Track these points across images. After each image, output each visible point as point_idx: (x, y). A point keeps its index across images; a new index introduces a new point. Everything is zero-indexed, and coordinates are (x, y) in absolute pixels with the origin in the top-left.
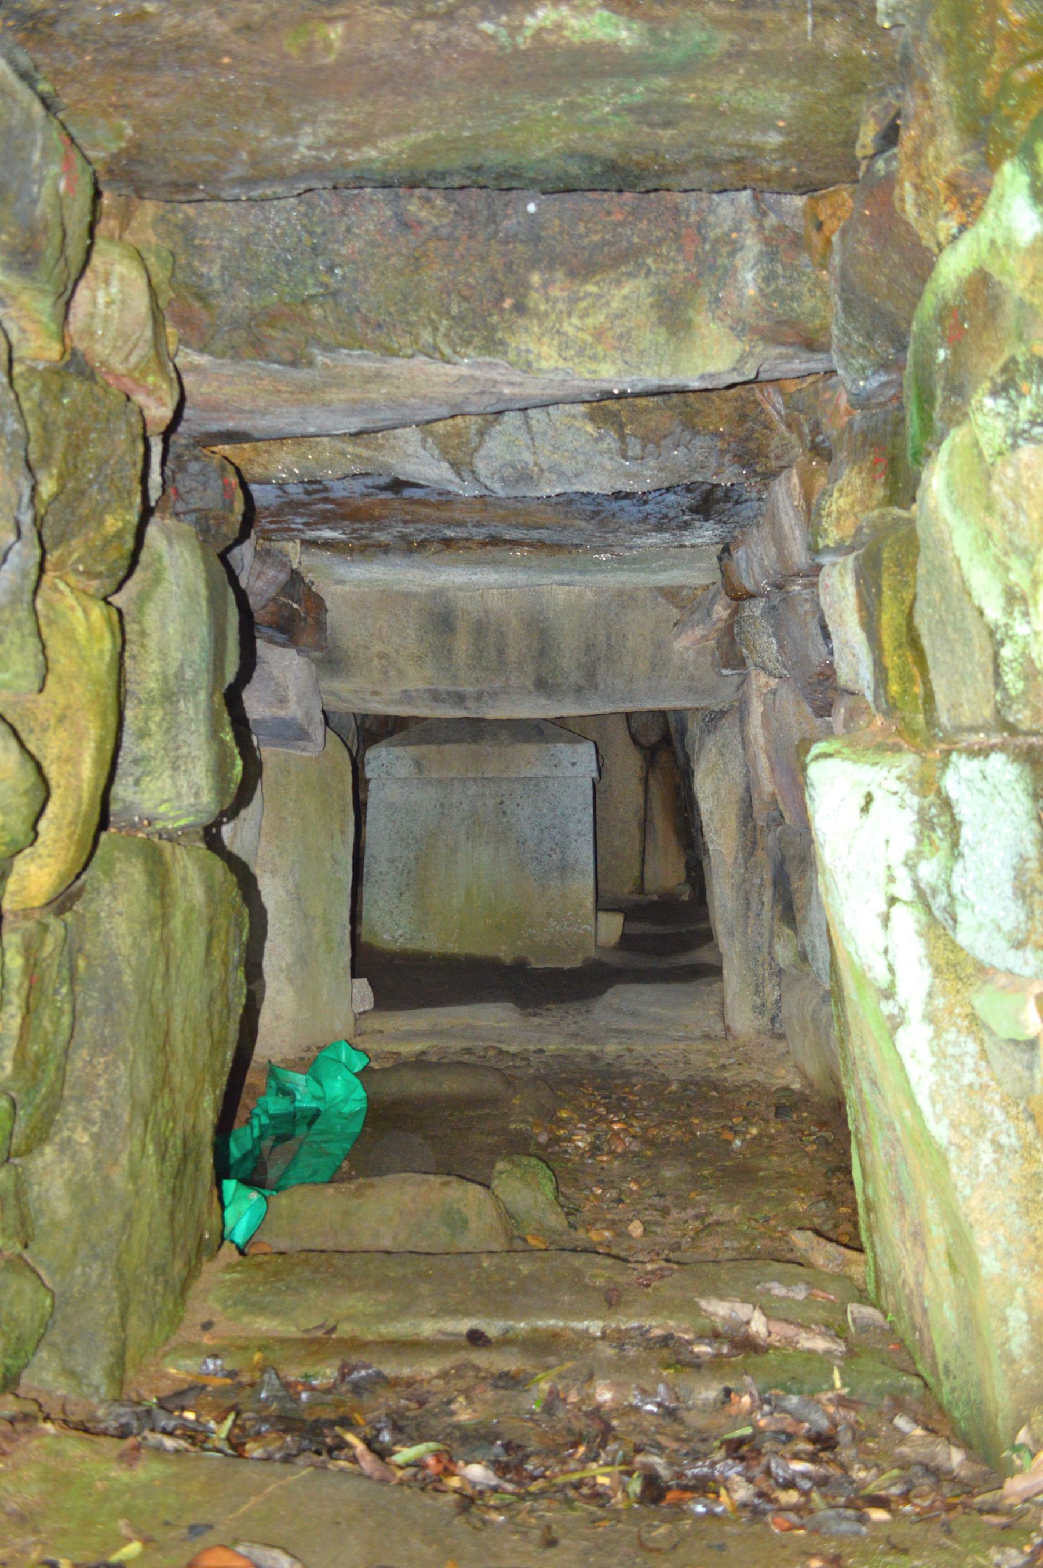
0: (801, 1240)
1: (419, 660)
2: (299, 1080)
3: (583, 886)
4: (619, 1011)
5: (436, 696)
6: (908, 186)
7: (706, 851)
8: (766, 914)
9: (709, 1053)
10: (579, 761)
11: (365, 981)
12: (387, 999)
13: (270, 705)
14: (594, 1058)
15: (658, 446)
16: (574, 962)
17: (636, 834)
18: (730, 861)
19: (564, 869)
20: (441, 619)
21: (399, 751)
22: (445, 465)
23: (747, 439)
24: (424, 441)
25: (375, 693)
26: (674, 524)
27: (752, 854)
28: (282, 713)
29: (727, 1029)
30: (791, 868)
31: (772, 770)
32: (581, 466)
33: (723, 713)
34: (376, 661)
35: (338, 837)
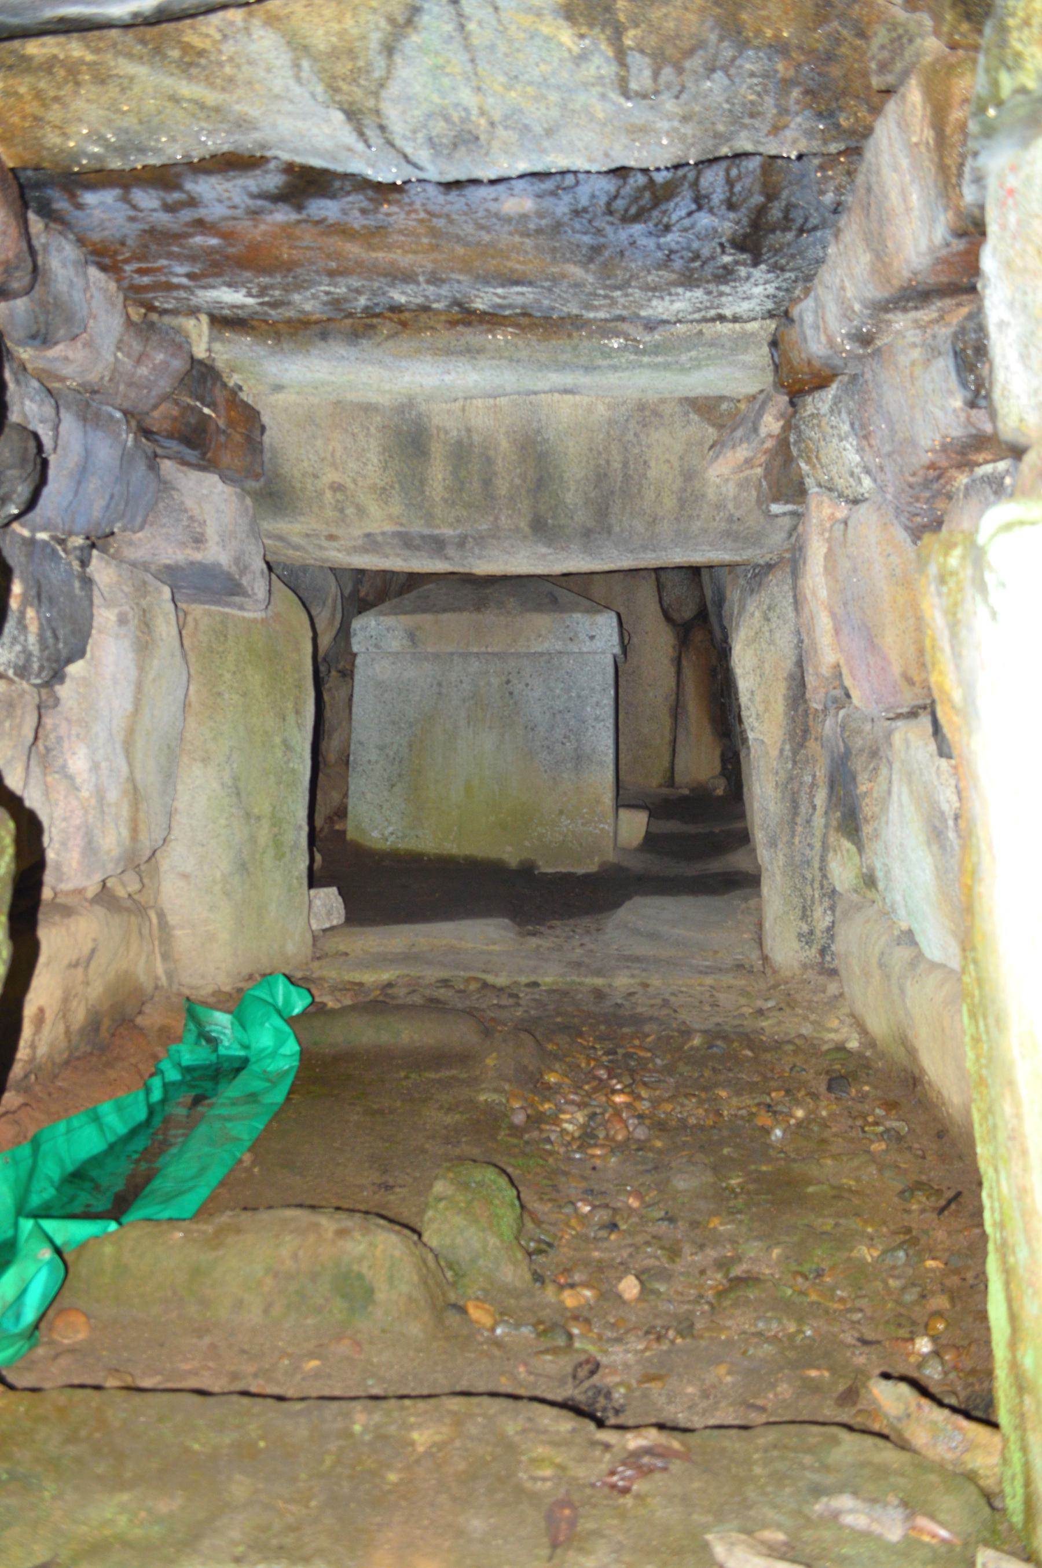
0: (891, 1399)
1: (383, 493)
2: (221, 1021)
3: (602, 779)
4: (636, 932)
5: (407, 542)
7: (745, 740)
8: (819, 820)
9: (744, 993)
10: (596, 636)
11: (334, 890)
12: (361, 911)
13: (183, 545)
14: (599, 994)
15: (680, 70)
16: (591, 867)
17: (667, 721)
18: (774, 753)
19: (580, 759)
20: (410, 438)
21: (390, 621)
22: (338, 117)
23: (830, 58)
24: (297, 66)
25: (331, 537)
26: (709, 270)
27: (802, 745)
28: (198, 556)
29: (765, 959)
30: (858, 764)
31: (837, 631)
32: (555, 113)
33: (769, 567)
34: (328, 494)
35: (291, 718)
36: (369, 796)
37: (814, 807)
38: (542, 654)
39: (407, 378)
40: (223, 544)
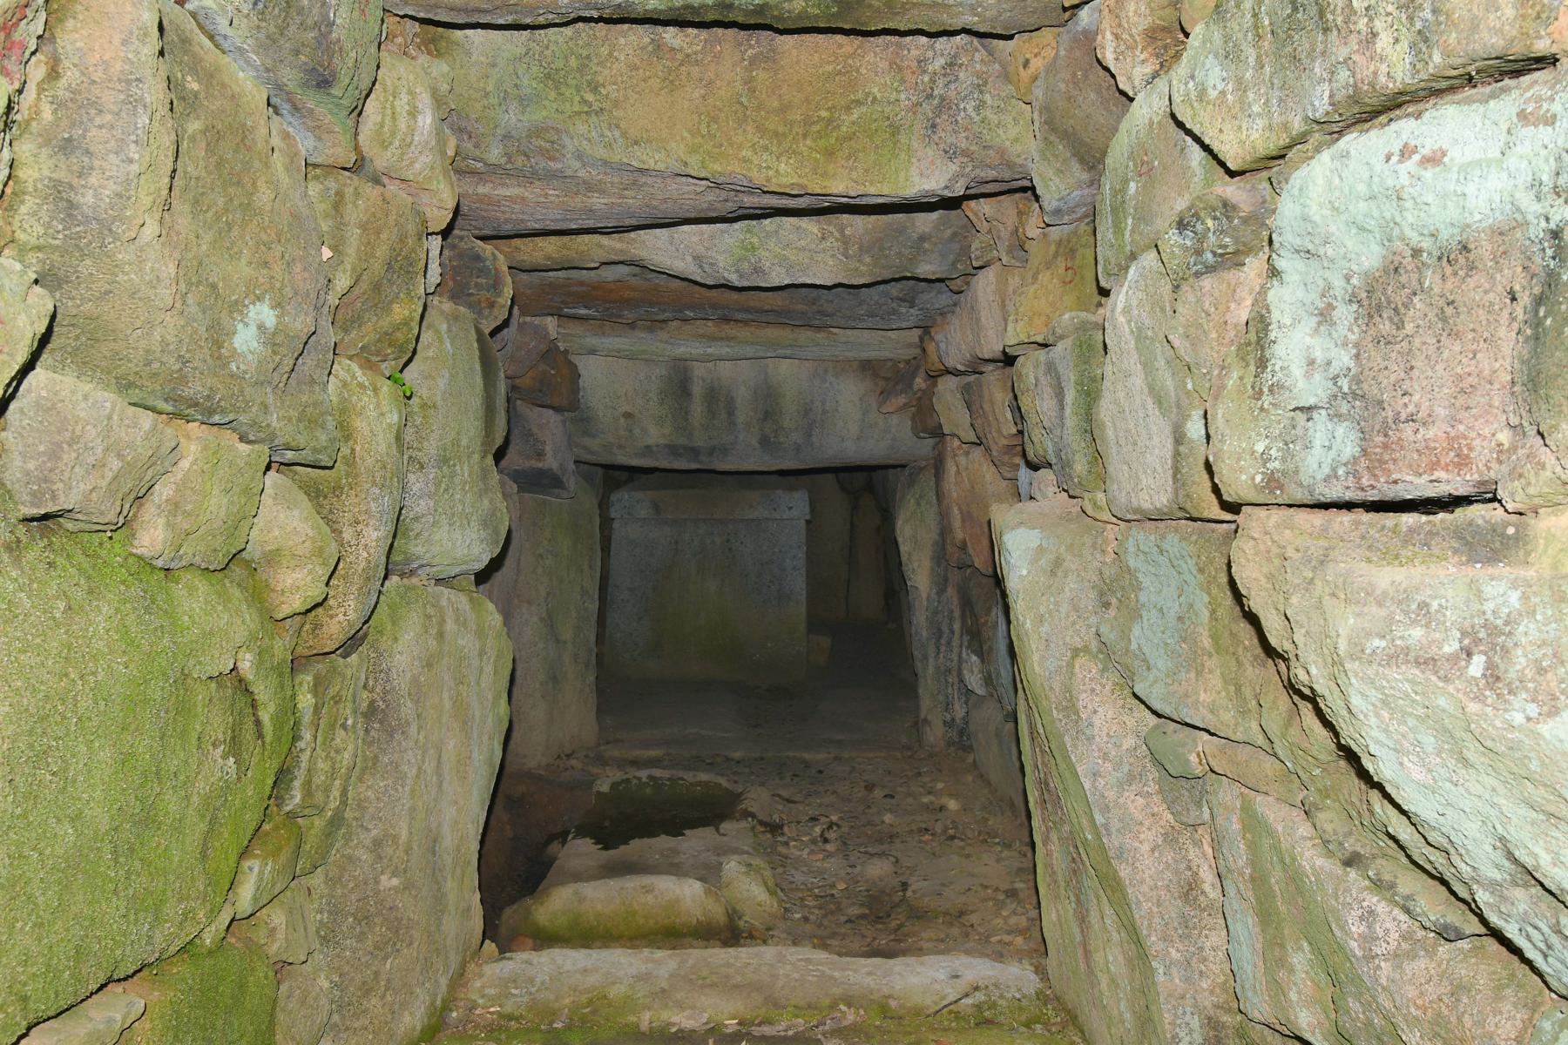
3: (798, 610)
6: (1109, 36)
10: (795, 506)
21: (639, 495)
31: (963, 521)
34: (622, 420)
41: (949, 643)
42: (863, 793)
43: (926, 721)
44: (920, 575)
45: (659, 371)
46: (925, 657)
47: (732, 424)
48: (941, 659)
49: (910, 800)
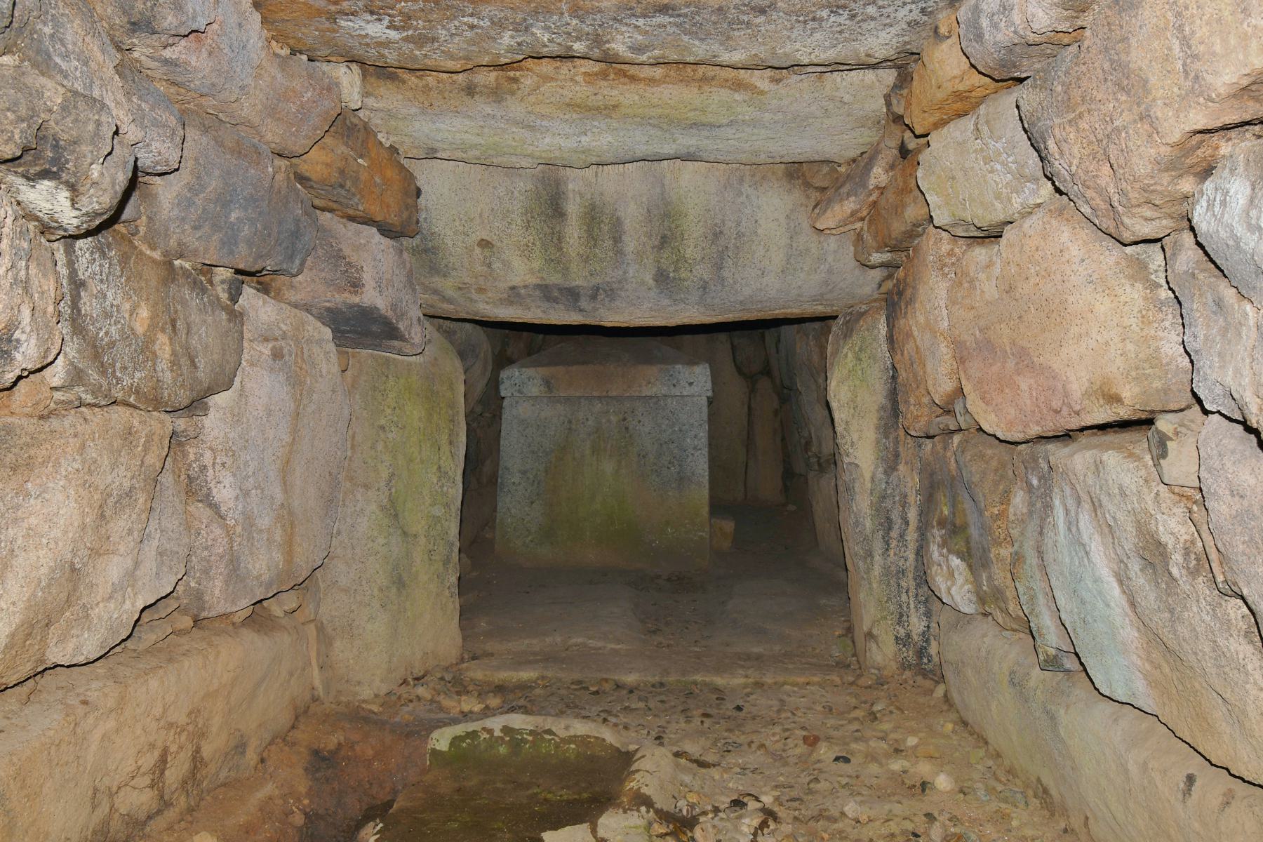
3: (701, 494)
13: (341, 290)
19: (682, 480)
21: (530, 372)
28: (356, 300)
34: (478, 250)
35: (445, 448)
36: (513, 511)
37: (907, 523)
38: (651, 397)
39: (547, 140)
40: (380, 288)
41: (902, 536)
42: (802, 749)
43: (870, 635)
44: (860, 446)
45: (524, 184)
46: (870, 554)
47: (620, 252)
48: (892, 557)
49: (874, 768)
